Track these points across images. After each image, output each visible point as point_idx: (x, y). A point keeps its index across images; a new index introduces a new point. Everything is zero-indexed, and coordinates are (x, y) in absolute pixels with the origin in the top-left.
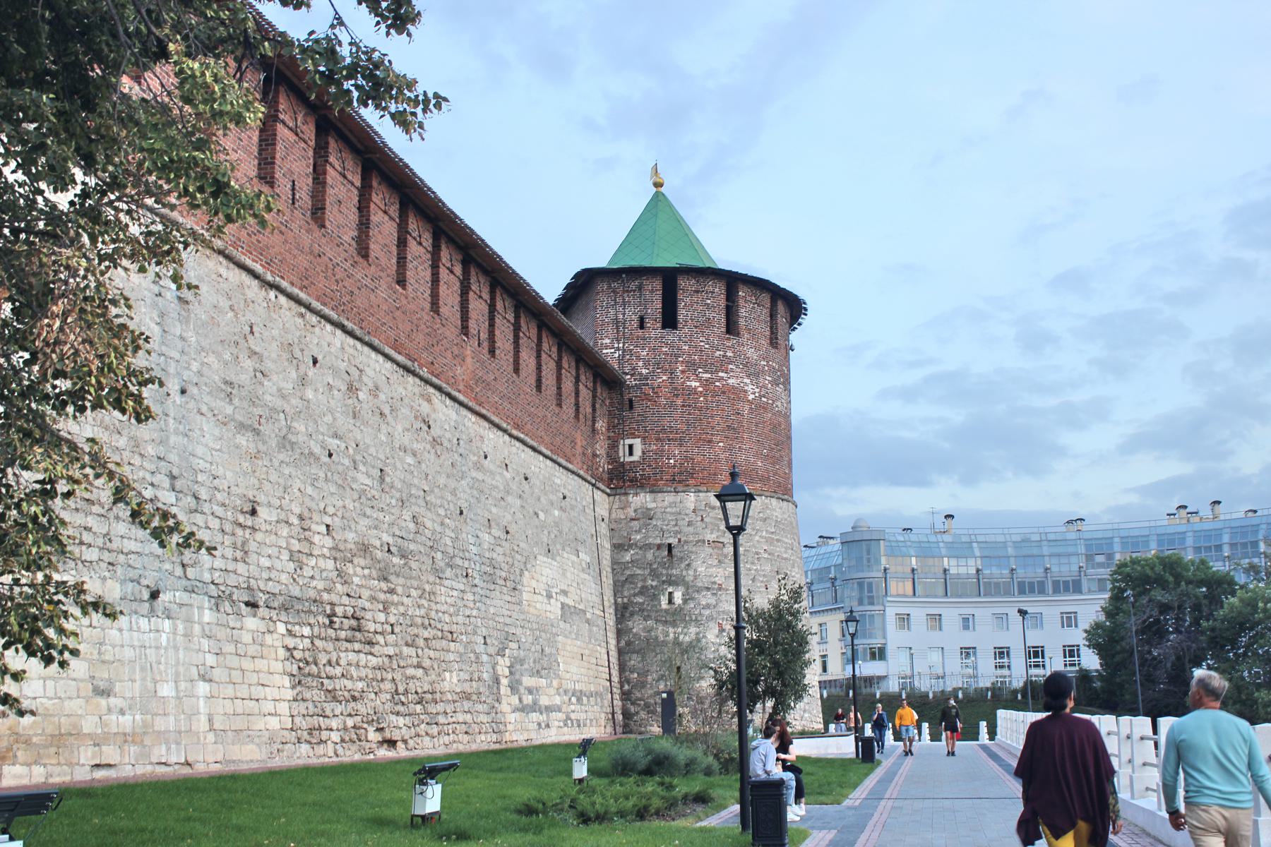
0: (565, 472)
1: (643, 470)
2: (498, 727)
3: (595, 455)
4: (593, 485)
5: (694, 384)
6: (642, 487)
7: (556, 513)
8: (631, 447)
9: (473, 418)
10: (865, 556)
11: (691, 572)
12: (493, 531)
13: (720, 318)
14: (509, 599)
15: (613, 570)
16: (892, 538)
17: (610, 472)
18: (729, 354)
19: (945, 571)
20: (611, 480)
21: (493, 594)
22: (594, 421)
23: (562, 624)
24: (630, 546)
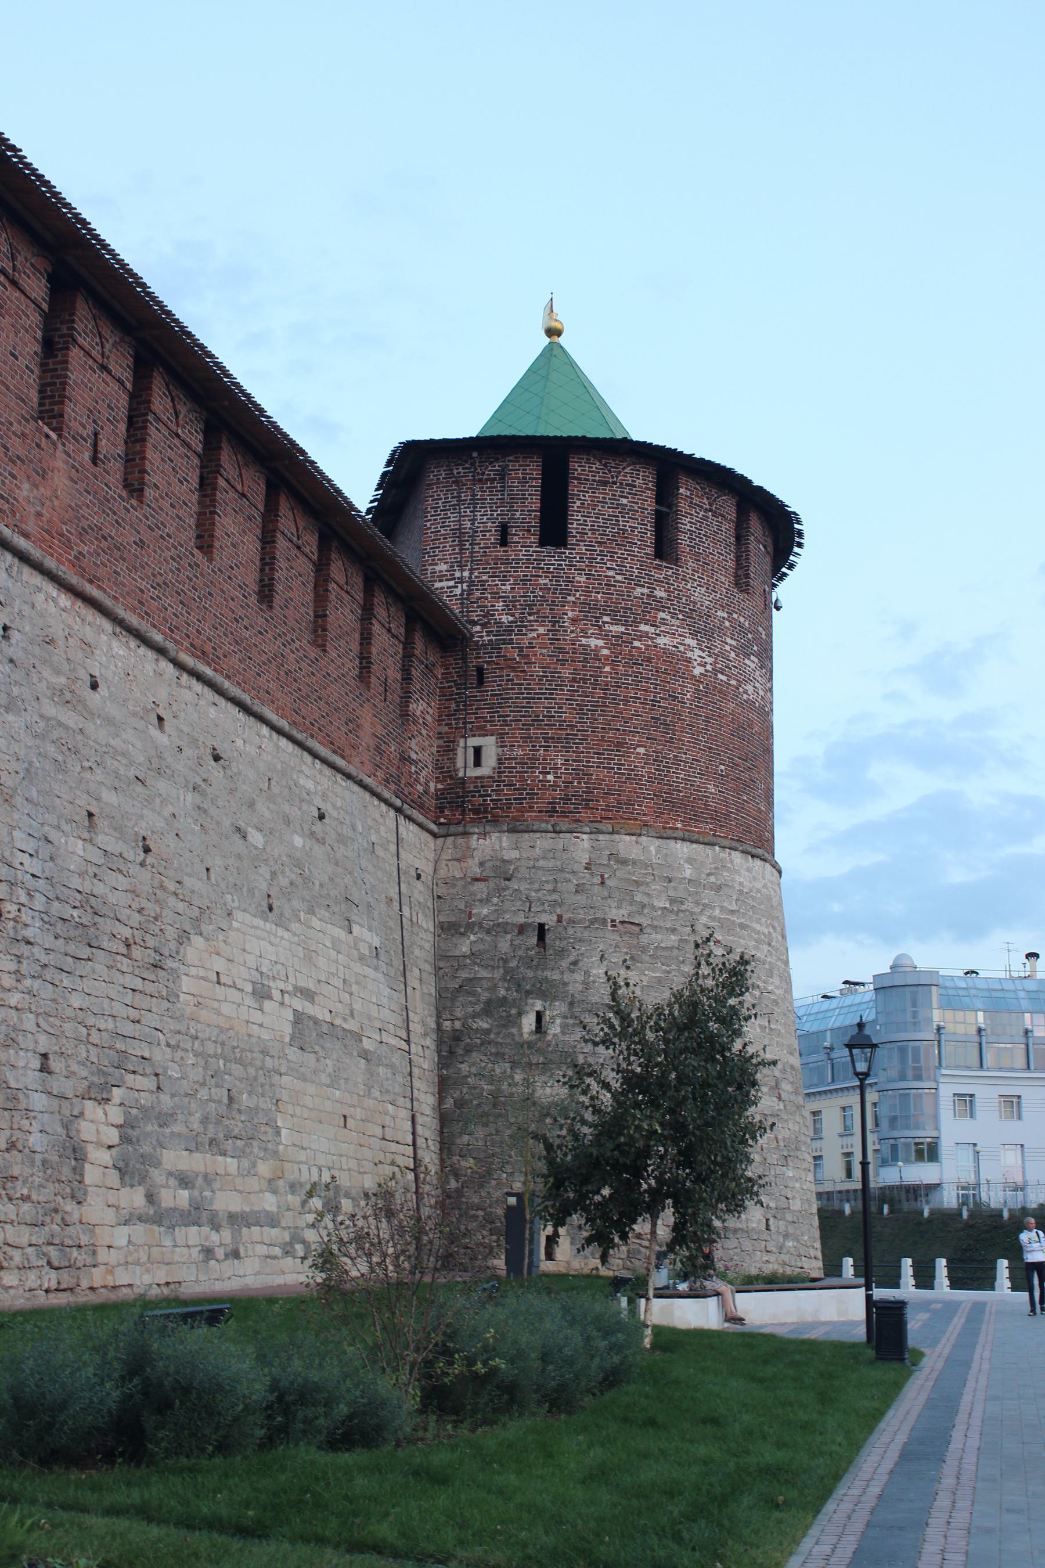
0: (328, 771)
1: (498, 792)
2: (65, 1253)
3: (405, 759)
4: (398, 810)
5: (594, 642)
6: (495, 821)
7: (298, 841)
8: (478, 751)
9: (65, 600)
10: (910, 1009)
11: (579, 977)
12: (100, 839)
13: (643, 532)
14: (138, 984)
15: (437, 969)
16: (949, 984)
17: (439, 795)
18: (660, 593)
19: (1027, 1032)
20: (441, 809)
21: (84, 968)
22: (406, 698)
23: (293, 1054)
24: (470, 927)
